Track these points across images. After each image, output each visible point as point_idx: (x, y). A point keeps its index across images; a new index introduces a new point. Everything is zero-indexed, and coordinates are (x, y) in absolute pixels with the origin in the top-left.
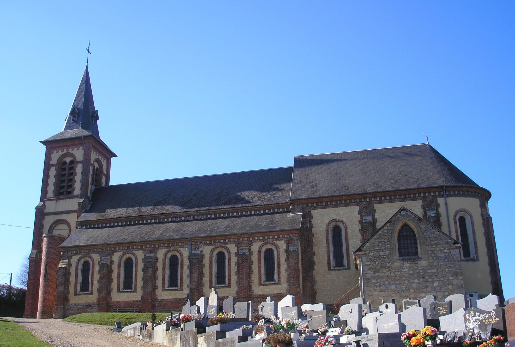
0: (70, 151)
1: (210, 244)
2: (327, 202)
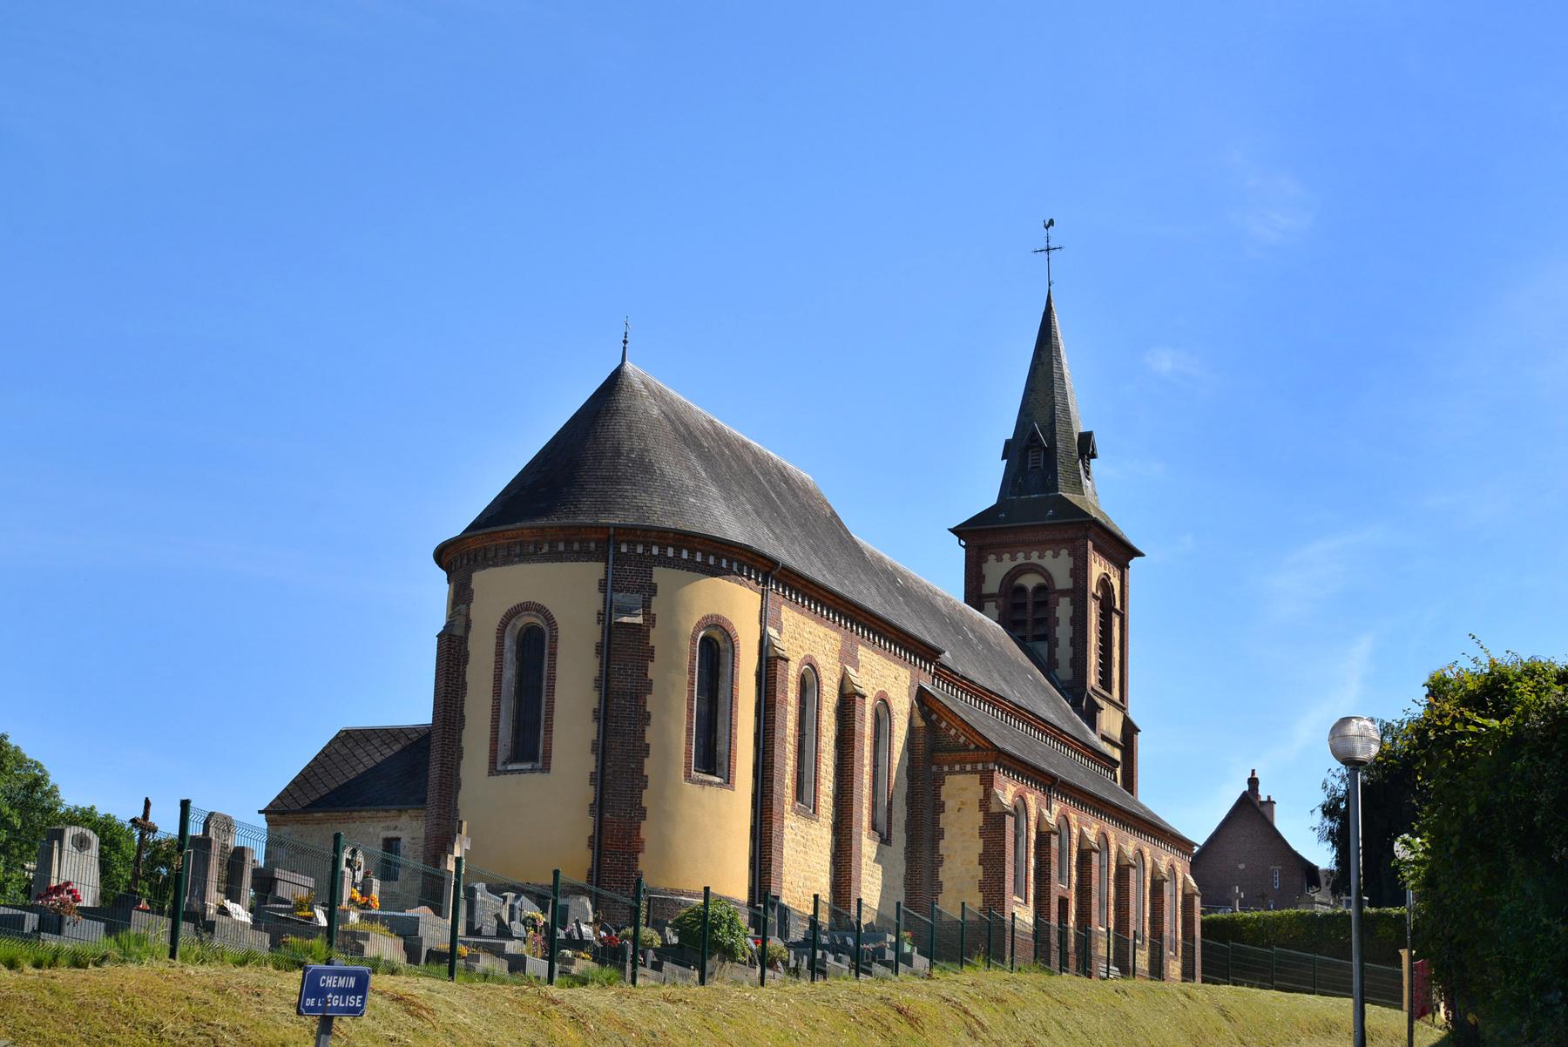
0: (1034, 557)
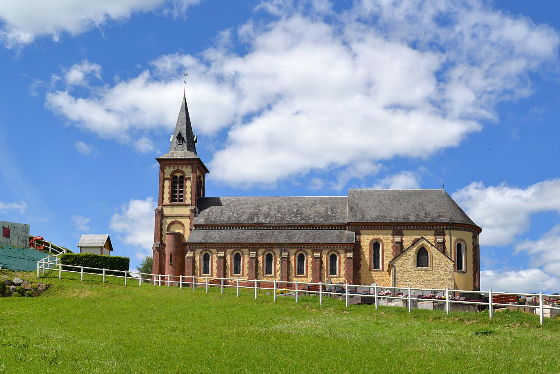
0: (180, 168)
1: (295, 248)
2: (371, 226)
